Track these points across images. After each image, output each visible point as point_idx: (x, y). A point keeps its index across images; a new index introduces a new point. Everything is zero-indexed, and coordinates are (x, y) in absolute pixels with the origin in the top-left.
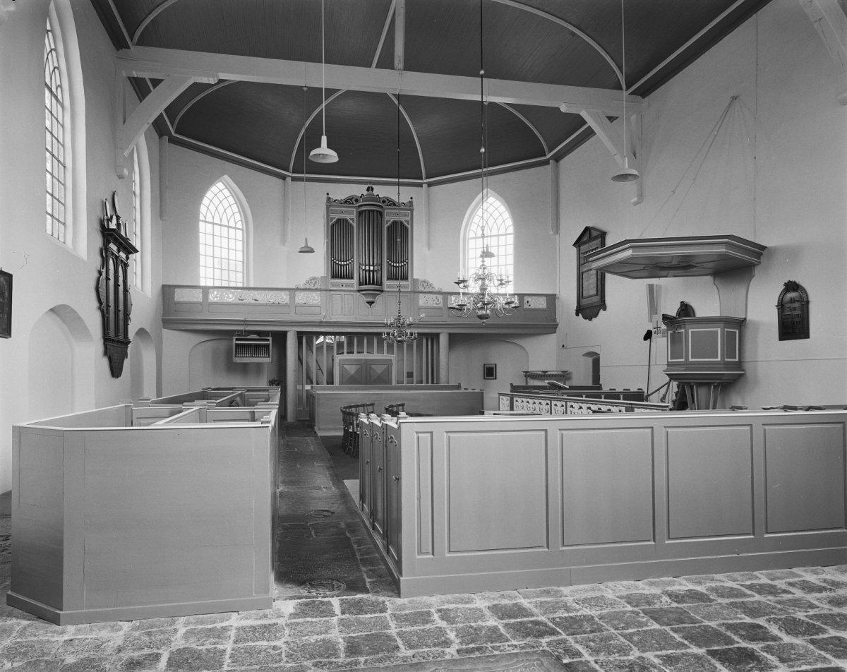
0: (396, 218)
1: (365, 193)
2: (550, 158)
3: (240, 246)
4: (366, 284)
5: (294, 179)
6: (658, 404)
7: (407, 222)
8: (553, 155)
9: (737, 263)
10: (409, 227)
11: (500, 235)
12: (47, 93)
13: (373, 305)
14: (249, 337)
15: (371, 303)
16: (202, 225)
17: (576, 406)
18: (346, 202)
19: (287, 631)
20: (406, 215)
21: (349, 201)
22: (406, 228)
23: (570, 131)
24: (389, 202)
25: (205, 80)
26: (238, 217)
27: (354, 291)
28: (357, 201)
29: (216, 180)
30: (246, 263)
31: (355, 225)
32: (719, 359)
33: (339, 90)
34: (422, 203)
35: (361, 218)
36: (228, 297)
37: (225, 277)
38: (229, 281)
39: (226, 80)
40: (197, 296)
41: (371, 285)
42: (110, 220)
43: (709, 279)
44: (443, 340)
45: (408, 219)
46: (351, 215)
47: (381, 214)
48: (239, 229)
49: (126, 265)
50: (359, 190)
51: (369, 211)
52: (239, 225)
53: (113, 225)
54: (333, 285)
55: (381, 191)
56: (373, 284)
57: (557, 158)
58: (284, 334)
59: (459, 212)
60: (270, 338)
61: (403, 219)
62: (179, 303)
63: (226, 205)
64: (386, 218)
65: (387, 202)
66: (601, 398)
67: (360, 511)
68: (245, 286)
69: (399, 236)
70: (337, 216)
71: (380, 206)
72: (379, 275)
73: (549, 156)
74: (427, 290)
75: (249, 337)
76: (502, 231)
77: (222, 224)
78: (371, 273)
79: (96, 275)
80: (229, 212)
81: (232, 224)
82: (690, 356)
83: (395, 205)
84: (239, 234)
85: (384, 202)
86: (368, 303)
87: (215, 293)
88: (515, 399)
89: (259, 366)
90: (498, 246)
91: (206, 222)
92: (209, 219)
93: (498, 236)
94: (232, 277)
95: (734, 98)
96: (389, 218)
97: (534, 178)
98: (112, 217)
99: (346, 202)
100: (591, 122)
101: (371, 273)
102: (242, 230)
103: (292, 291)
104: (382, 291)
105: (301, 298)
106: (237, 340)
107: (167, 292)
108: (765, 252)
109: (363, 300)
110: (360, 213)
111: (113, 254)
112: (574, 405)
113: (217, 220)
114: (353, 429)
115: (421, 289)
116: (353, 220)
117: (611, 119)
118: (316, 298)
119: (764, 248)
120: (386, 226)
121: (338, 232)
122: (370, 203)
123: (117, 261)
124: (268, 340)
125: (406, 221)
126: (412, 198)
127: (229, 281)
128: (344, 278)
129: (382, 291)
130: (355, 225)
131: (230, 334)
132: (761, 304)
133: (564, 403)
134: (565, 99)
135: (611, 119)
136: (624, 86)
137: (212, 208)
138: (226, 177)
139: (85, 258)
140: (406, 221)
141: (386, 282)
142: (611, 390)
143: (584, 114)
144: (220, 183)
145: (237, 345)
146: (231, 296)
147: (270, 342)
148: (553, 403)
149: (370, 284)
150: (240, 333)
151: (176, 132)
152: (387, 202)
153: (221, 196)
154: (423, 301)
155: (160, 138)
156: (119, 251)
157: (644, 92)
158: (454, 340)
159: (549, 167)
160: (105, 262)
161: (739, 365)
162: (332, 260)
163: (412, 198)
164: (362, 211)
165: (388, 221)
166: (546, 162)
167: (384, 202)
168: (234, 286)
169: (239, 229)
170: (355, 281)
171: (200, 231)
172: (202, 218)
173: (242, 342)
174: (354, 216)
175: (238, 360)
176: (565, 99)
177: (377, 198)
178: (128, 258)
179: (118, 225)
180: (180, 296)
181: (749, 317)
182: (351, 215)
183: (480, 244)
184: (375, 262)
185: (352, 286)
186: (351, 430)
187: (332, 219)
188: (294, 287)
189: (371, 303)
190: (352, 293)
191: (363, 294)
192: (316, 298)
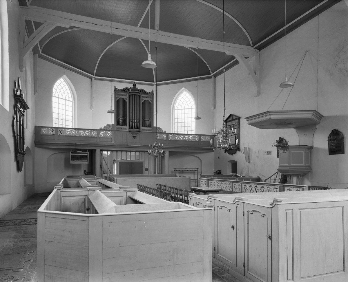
0: (147, 99)
1: (132, 87)
2: (213, 76)
3: (71, 109)
4: (133, 128)
5: (96, 79)
6: (296, 185)
7: (151, 101)
8: (214, 75)
9: (306, 125)
11: (189, 109)
14: (77, 152)
16: (53, 98)
17: (248, 185)
18: (123, 90)
19: (10, 272)
20: (150, 98)
21: (126, 90)
22: (151, 104)
23: (227, 62)
24: (143, 92)
25: (63, 26)
26: (70, 95)
27: (127, 131)
28: (128, 90)
29: (60, 77)
30: (74, 117)
31: (127, 101)
32: (304, 164)
33: (123, 36)
34: (161, 92)
35: (130, 98)
36: (75, 132)
37: (64, 123)
38: (66, 125)
39: (78, 28)
40: (50, 132)
41: (134, 129)
42: (17, 91)
43: (293, 130)
45: (151, 99)
46: (126, 97)
47: (139, 96)
48: (70, 101)
49: (23, 115)
50: (130, 86)
51: (134, 95)
52: (71, 99)
53: (19, 94)
54: (117, 128)
55: (139, 87)
56: (136, 128)
57: (215, 76)
59: (172, 96)
60: (88, 153)
61: (149, 99)
62: (43, 135)
63: (64, 89)
64: (142, 98)
66: (243, 181)
68: (73, 127)
69: (148, 108)
70: (119, 97)
71: (139, 93)
72: (138, 124)
74: (160, 132)
75: (77, 152)
76: (190, 107)
77: (63, 98)
78: (135, 124)
79: (12, 119)
80: (66, 92)
81: (67, 99)
82: (291, 163)
84: (71, 103)
85: (141, 91)
86: (133, 137)
88: (210, 181)
89: (79, 166)
90: (181, 114)
91: (55, 97)
92: (57, 96)
93: (181, 109)
94: (67, 124)
95: (306, 52)
97: (205, 84)
98: (18, 90)
100: (238, 58)
101: (135, 124)
102: (72, 101)
103: (98, 131)
104: (140, 132)
105: (102, 134)
106: (72, 153)
107: (37, 130)
108: (323, 119)
109: (130, 135)
110: (130, 96)
111: (19, 109)
112: (236, 184)
113: (60, 96)
114: (174, 195)
117: (246, 58)
118: (102, 134)
119: (323, 116)
120: (141, 102)
121: (120, 104)
122: (137, 91)
123: (20, 112)
124: (87, 153)
125: (150, 100)
126: (153, 90)
127: (66, 125)
129: (140, 132)
130: (127, 101)
131: (68, 150)
132: (321, 141)
133: (240, 184)
134: (230, 49)
135: (246, 58)
136: (252, 44)
137: (58, 90)
138: (65, 76)
139: (8, 109)
140: (150, 100)
141: (142, 128)
142: (250, 177)
143: (235, 55)
144: (62, 79)
145: (72, 155)
146: (74, 133)
147: (88, 154)
148: (243, 184)
149: (134, 128)
150: (73, 150)
151: (42, 52)
153: (62, 84)
155: (34, 55)
156: (21, 108)
157: (260, 48)
158: (171, 154)
159: (212, 80)
160: (15, 113)
161: (310, 167)
162: (117, 117)
163: (153, 90)
164: (131, 95)
165: (142, 100)
166: (210, 77)
167: (141, 91)
168: (61, 127)
169: (70, 101)
170: (127, 127)
171: (53, 101)
172: (53, 95)
173: (74, 154)
175: (72, 163)
176: (230, 49)
177: (137, 89)
178: (24, 112)
179: (21, 94)
180: (44, 131)
181: (315, 145)
182: (126, 97)
183: (181, 112)
184: (137, 119)
185: (126, 129)
186: (177, 197)
187: (117, 98)
188: (99, 129)
189: (134, 137)
191: (131, 133)
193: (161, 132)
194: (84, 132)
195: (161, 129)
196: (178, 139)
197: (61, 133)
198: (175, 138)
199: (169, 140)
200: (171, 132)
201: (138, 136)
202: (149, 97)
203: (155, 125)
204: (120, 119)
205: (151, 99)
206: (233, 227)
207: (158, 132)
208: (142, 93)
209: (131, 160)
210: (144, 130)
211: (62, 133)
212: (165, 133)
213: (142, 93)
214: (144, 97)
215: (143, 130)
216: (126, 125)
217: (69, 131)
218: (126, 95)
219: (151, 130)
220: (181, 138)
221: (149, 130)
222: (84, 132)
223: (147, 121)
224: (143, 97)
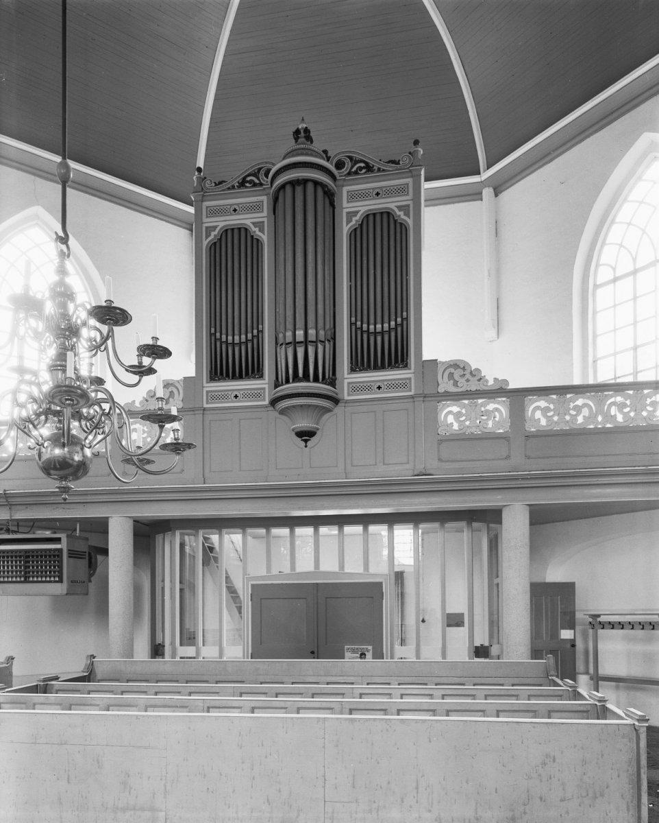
2: (483, 184)
10: (410, 222)
12: (242, 558)
13: (313, 440)
15: (306, 435)
18: (242, 184)
20: (402, 190)
22: (403, 227)
31: (265, 238)
44: (516, 525)
45: (405, 200)
46: (252, 214)
47: (330, 196)
54: (213, 397)
58: (101, 527)
65: (348, 164)
67: (78, 399)
70: (221, 222)
73: (486, 175)
74: (463, 386)
78: (379, 339)
83: (369, 168)
87: (490, 424)
96: (354, 205)
99: (242, 184)
101: (379, 339)
115: (445, 386)
116: (260, 225)
125: (400, 208)
128: (241, 377)
129: (336, 401)
141: (347, 378)
152: (348, 164)
154: (451, 416)
165: (351, 215)
166: (474, 195)
174: (264, 216)
182: (252, 214)
187: (209, 230)
189: (306, 435)
190: (207, 422)
192: (451, 419)
193: (473, 387)
194: (600, 403)
195: (475, 374)
196: (592, 417)
197: (456, 384)
198: (574, 417)
199: (528, 437)
200: (577, 381)
201: (330, 426)
202: (390, 192)
203: (427, 355)
204: (221, 343)
205: (405, 200)
206: (423, 621)
207: (453, 389)
208: (349, 174)
209: (317, 572)
210: (366, 388)
211: (462, 382)
212: (501, 391)
213: (349, 174)
214: (363, 196)
215: (355, 388)
216: (254, 370)
217: (585, 405)
218: (256, 207)
219: (404, 384)
220: (613, 411)
221: (394, 385)
222: (600, 403)
223: (382, 333)
224: (353, 197)
